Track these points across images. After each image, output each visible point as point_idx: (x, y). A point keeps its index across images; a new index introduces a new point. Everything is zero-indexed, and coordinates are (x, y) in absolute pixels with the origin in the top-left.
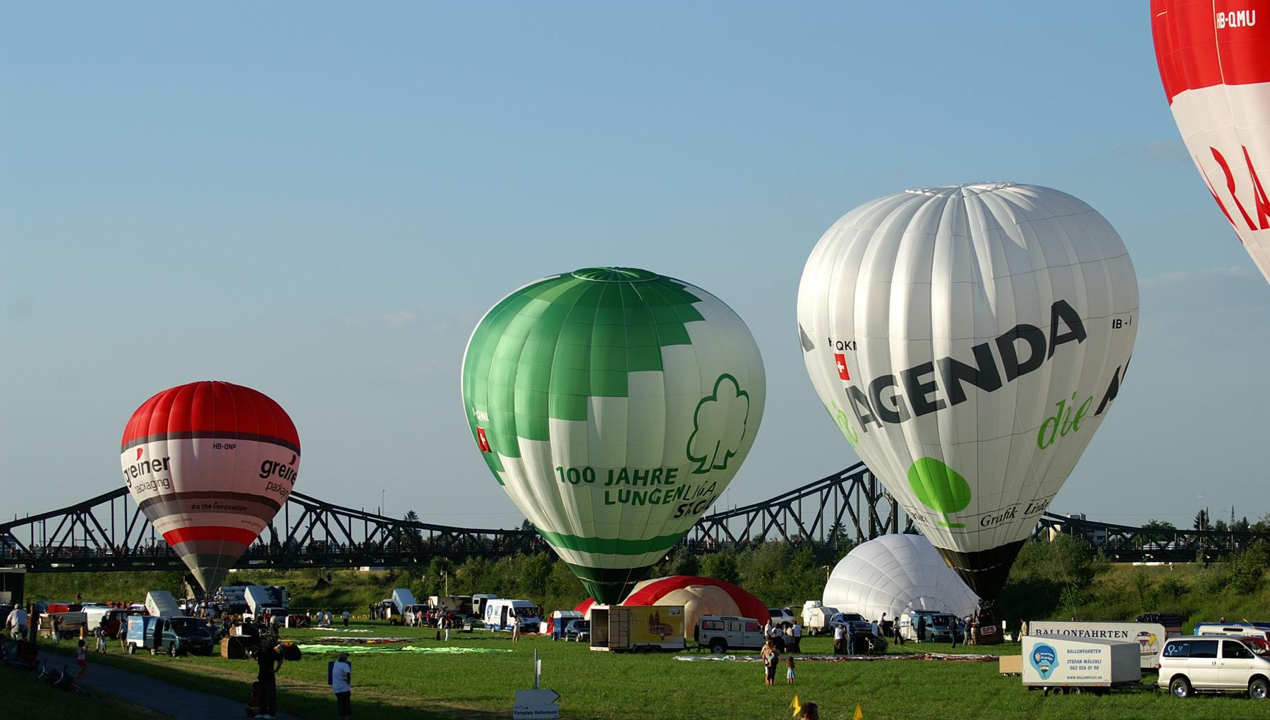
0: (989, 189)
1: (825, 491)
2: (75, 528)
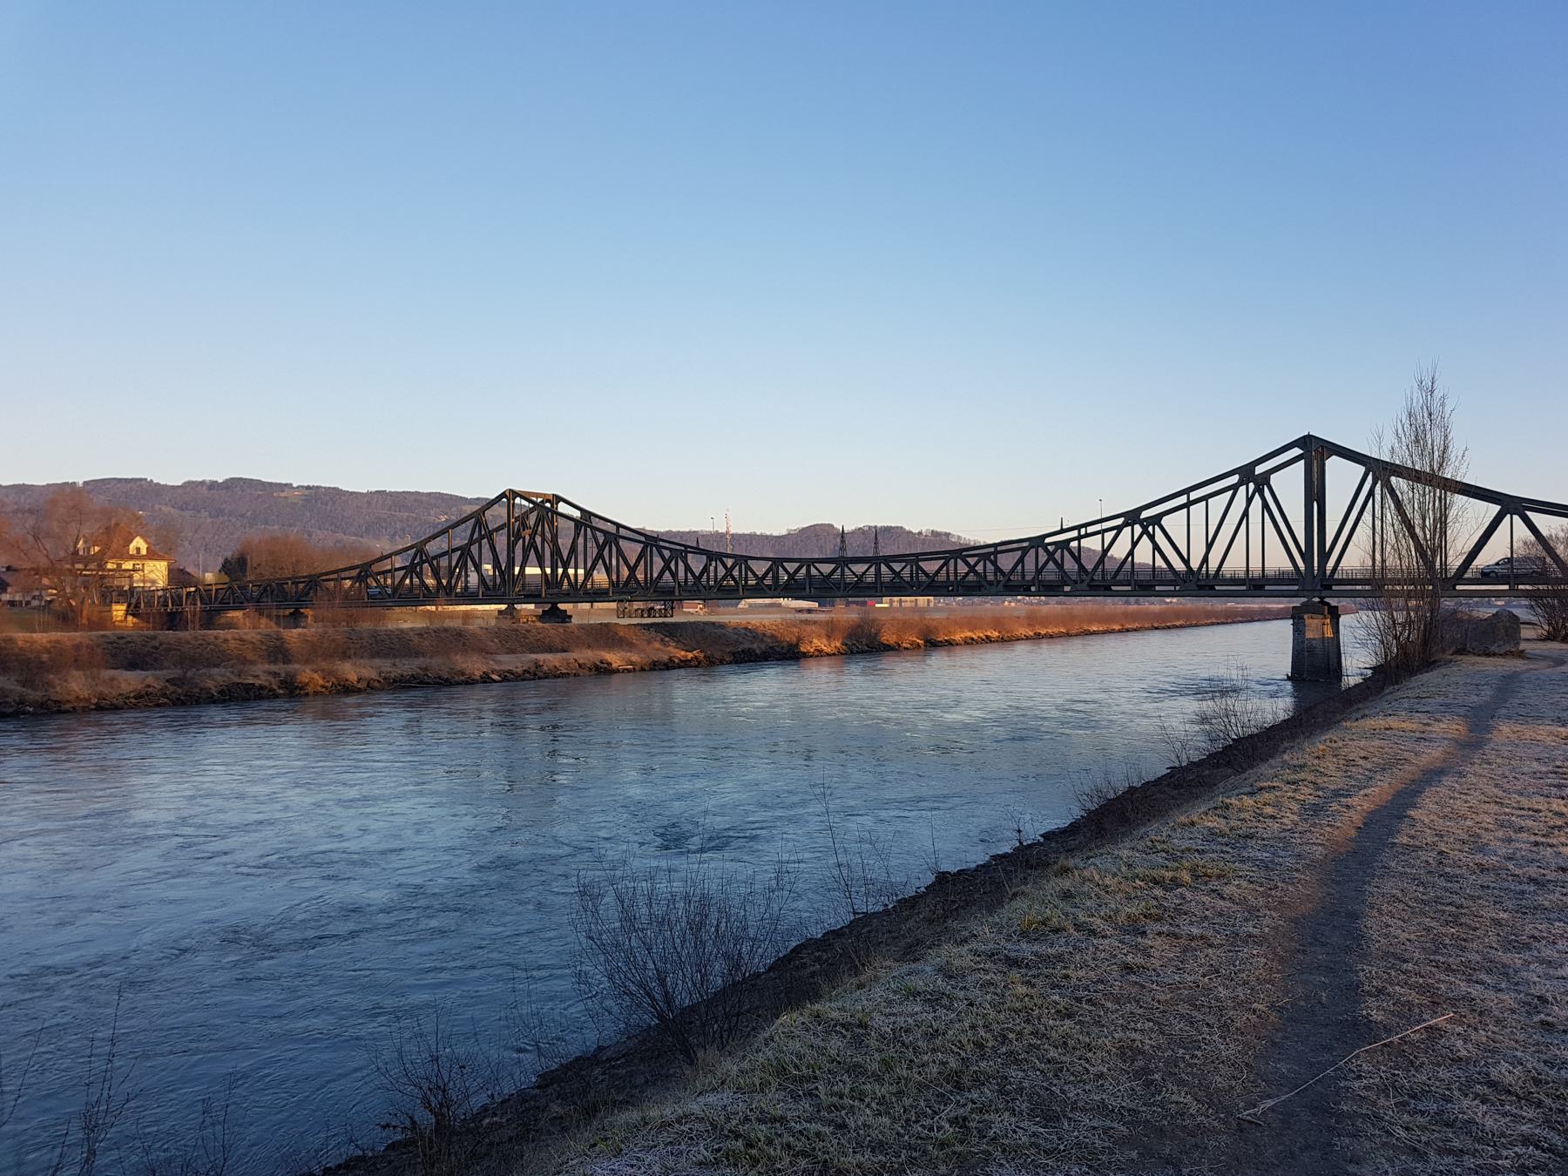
0: (93, 791)
1: (1109, 536)
2: (1135, 550)
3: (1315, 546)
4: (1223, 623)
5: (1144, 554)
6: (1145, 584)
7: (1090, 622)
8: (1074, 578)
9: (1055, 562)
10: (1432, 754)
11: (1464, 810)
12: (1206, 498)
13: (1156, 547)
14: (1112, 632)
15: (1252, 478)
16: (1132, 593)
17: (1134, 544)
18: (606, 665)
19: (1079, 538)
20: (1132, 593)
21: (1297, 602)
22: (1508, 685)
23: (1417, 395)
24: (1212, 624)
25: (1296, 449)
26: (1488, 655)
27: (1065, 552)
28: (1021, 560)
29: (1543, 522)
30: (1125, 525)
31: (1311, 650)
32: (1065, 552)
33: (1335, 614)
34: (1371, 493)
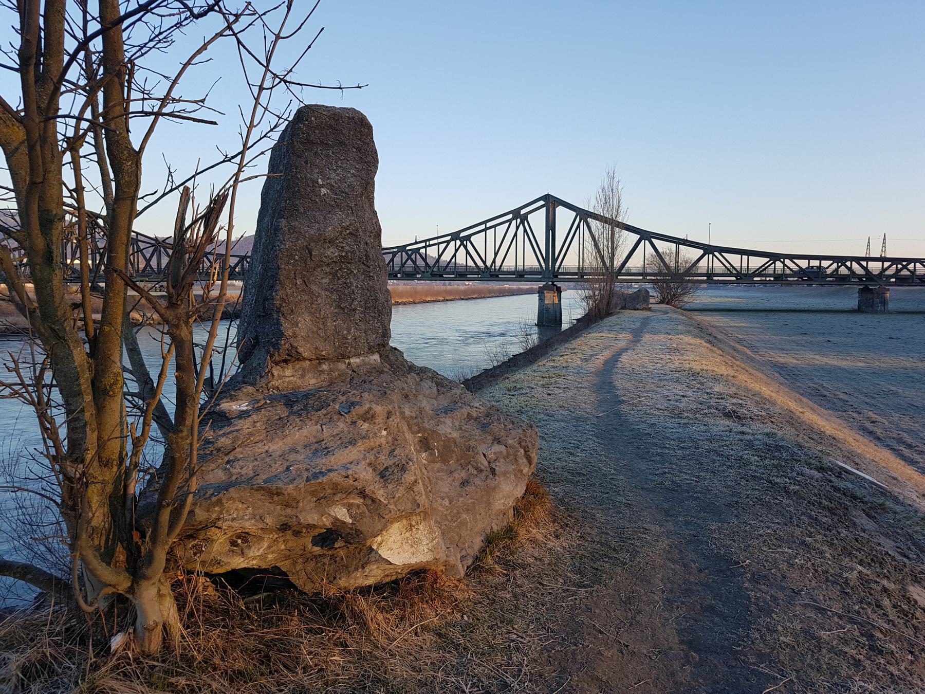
1: (442, 246)
3: (551, 256)
4: (498, 296)
5: (461, 258)
6: (462, 274)
7: (426, 296)
8: (423, 270)
9: (412, 260)
10: (622, 344)
11: (638, 358)
12: (494, 226)
13: (468, 252)
14: (438, 301)
15: (519, 216)
16: (455, 279)
17: (456, 250)
18: (136, 321)
19: (426, 247)
20: (455, 279)
21: (541, 284)
22: (645, 322)
23: (606, 180)
24: (492, 297)
25: (542, 201)
26: (635, 310)
27: (418, 255)
28: (392, 260)
29: (661, 245)
30: (452, 240)
31: (548, 310)
32: (418, 255)
33: (559, 291)
34: (578, 226)
